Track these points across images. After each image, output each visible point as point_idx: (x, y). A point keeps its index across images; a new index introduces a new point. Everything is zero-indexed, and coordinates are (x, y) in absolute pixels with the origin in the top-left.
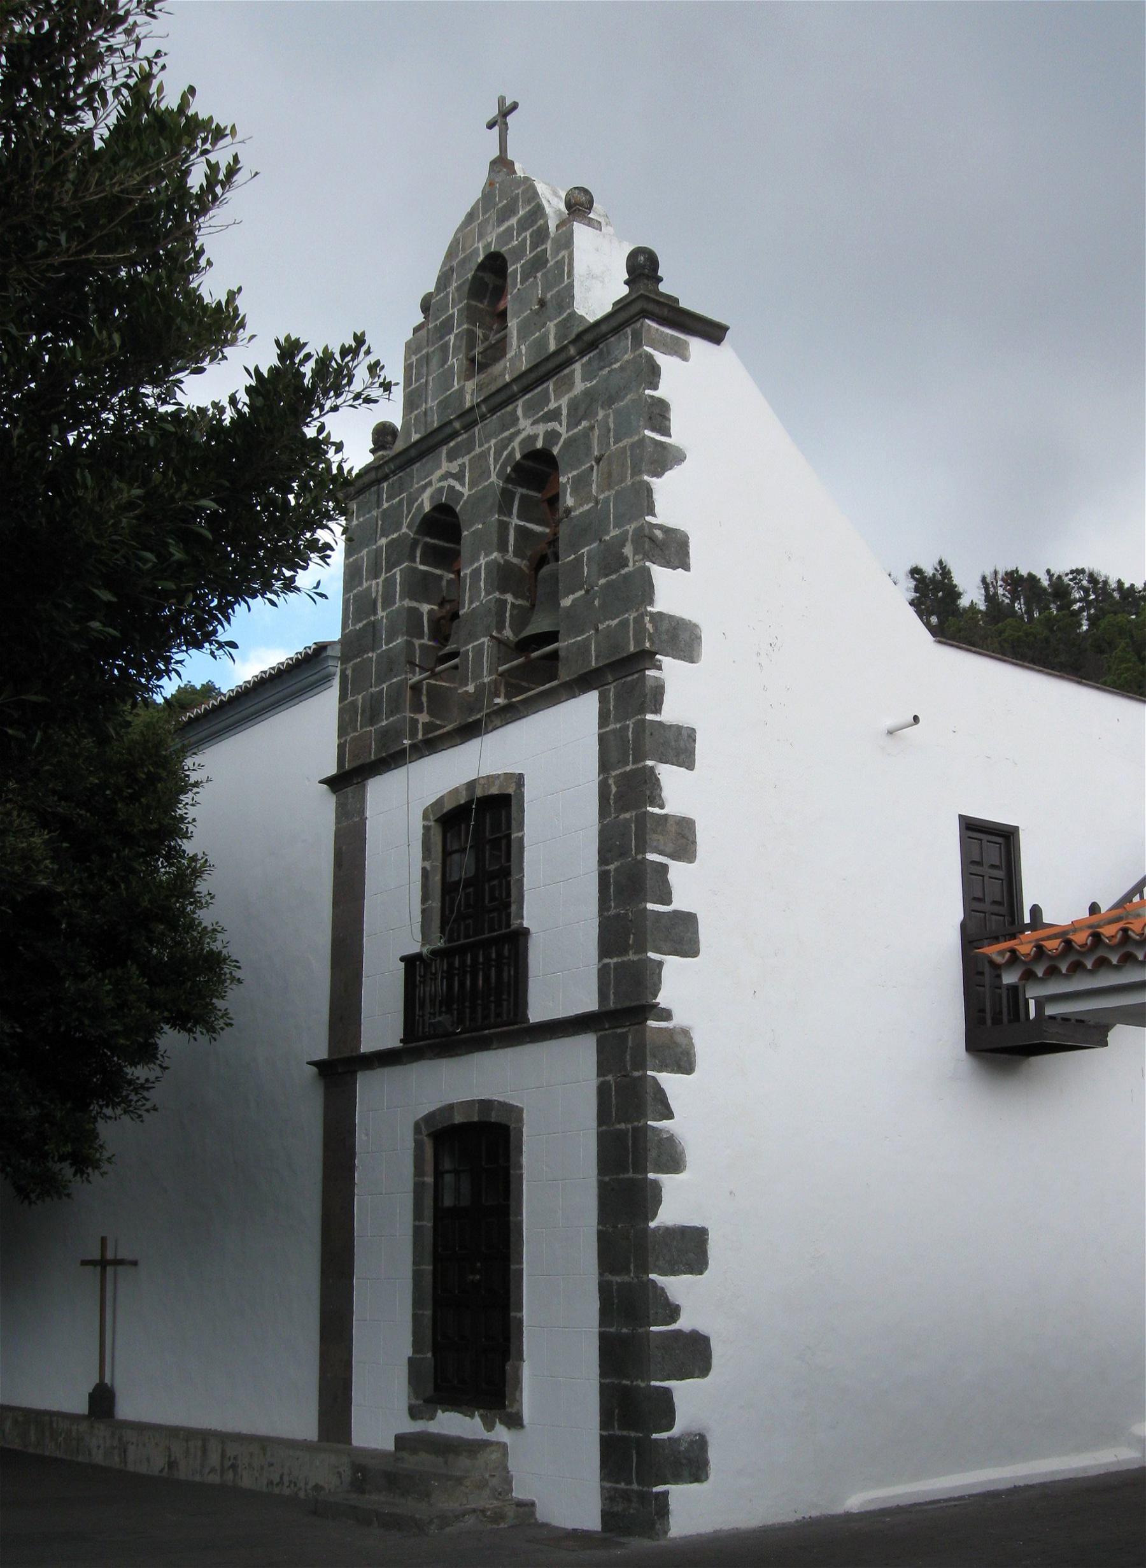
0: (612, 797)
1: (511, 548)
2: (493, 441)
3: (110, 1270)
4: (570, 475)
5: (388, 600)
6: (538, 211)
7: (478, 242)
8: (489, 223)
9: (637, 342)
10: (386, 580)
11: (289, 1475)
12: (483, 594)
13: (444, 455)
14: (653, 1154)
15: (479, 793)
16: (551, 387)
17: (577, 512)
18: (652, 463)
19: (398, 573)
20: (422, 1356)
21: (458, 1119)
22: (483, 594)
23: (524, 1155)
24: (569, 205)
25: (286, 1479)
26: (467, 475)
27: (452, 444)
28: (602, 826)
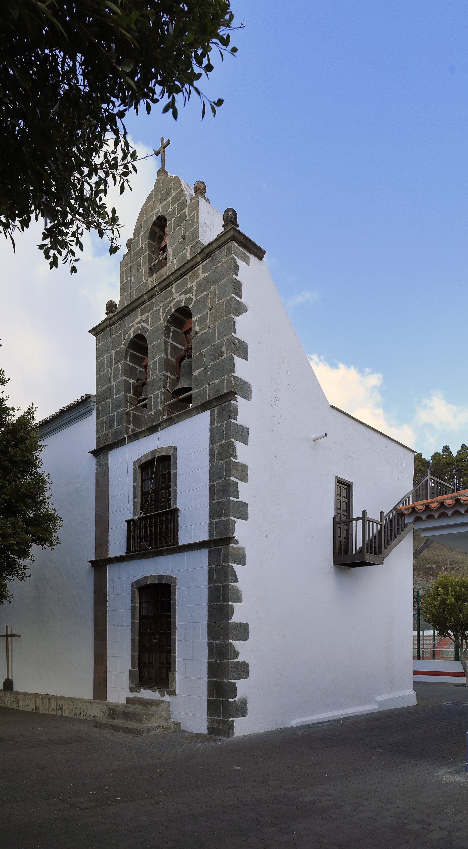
0: (215, 454)
1: (169, 353)
2: (162, 304)
3: (10, 638)
4: (197, 317)
5: (116, 377)
6: (181, 193)
7: (153, 211)
8: (158, 201)
9: (230, 251)
10: (115, 368)
11: (83, 712)
12: (158, 372)
13: (139, 312)
14: (231, 595)
15: (157, 455)
16: (188, 277)
17: (200, 334)
18: (235, 310)
19: (120, 365)
20: (135, 669)
21: (149, 582)
22: (158, 372)
23: (177, 596)
24: (196, 191)
25: (82, 713)
26: (150, 320)
27: (143, 307)
28: (211, 467)
